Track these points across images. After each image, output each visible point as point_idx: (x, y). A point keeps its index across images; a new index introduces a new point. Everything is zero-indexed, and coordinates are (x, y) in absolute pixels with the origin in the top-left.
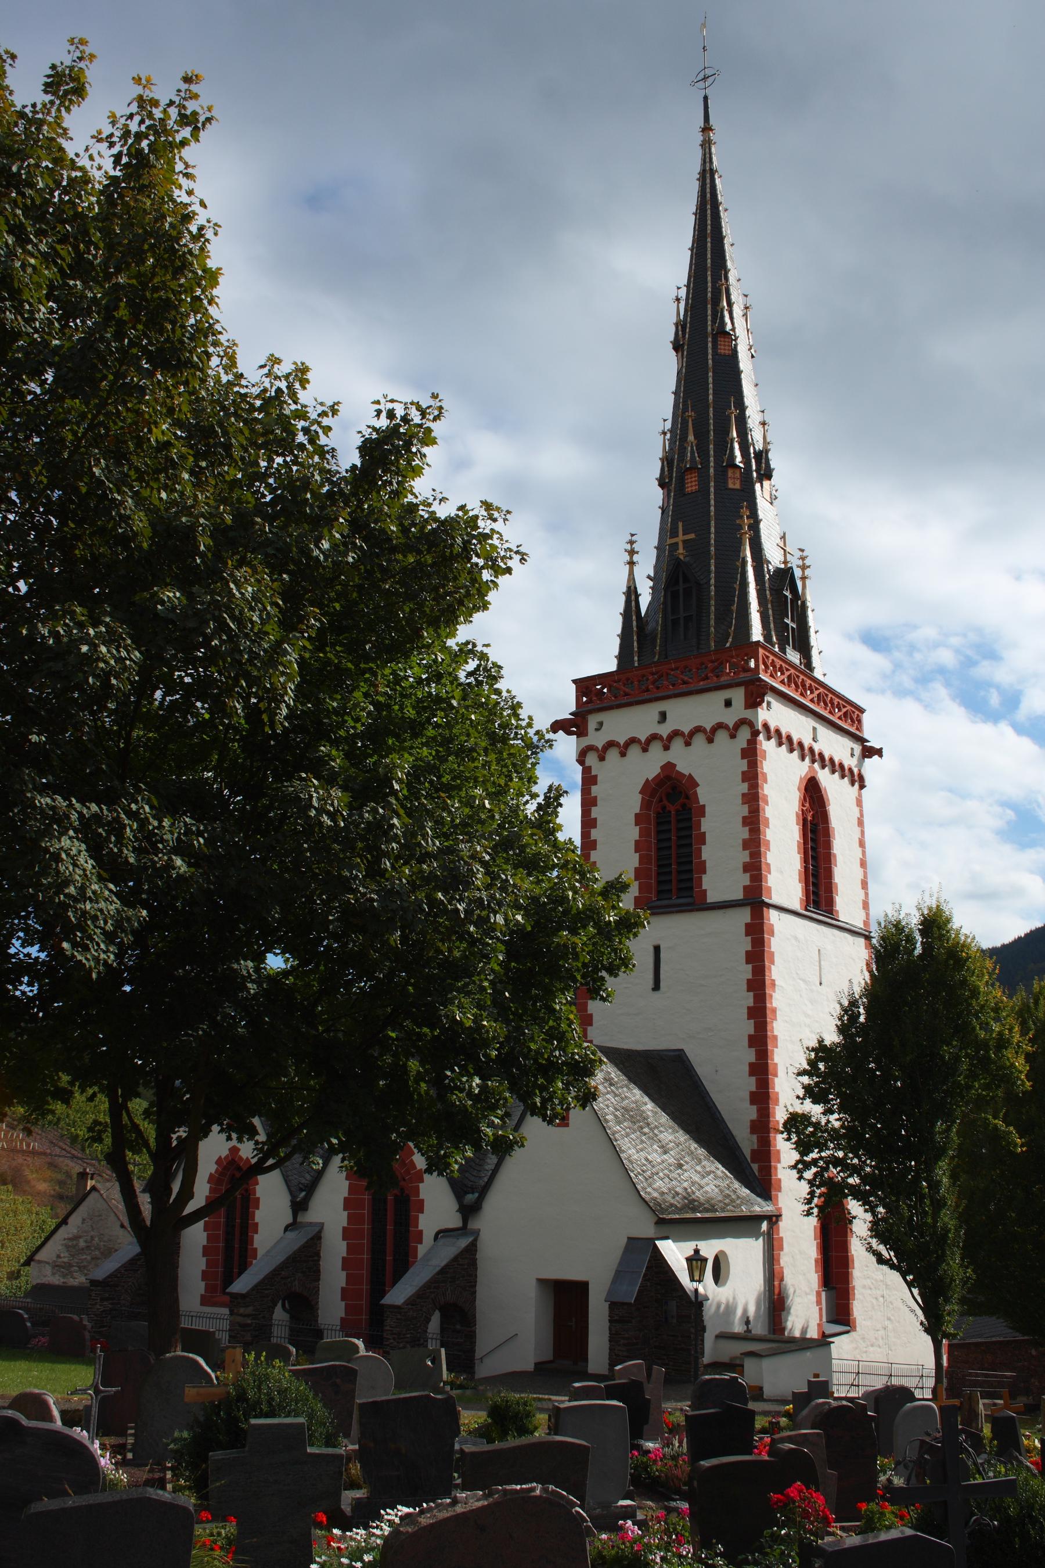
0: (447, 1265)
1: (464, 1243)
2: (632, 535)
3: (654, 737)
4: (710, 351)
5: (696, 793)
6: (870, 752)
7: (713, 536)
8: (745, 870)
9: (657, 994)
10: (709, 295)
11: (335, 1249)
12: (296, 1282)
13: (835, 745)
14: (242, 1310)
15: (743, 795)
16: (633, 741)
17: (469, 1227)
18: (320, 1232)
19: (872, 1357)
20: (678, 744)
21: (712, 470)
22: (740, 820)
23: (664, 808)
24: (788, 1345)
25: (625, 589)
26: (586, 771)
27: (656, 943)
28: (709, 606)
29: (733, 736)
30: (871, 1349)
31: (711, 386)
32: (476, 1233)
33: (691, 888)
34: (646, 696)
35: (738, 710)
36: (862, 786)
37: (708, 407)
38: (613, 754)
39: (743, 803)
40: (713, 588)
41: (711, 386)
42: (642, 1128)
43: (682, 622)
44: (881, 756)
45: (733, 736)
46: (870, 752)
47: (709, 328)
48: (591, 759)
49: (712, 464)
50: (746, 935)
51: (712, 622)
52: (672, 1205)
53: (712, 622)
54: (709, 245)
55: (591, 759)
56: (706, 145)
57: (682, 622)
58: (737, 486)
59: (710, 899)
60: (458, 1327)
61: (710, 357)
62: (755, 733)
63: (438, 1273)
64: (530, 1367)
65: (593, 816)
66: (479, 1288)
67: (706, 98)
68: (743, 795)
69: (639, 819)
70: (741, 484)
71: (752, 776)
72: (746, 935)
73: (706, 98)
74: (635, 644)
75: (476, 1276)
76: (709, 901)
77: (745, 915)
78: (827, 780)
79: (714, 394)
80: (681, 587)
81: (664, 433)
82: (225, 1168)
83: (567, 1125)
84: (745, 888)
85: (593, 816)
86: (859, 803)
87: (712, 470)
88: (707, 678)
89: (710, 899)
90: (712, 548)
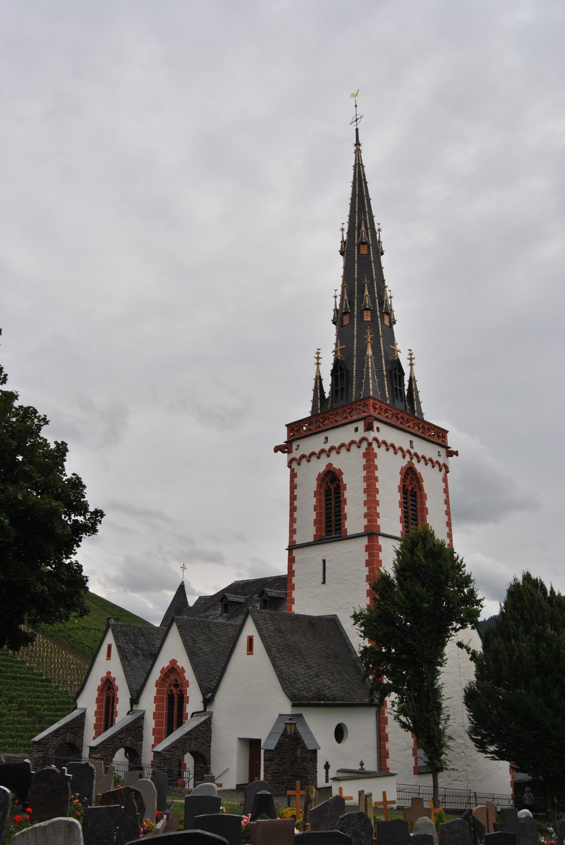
0: (191, 731)
1: (203, 719)
2: (318, 349)
3: (323, 451)
4: (356, 253)
5: (342, 478)
6: (451, 454)
7: (355, 346)
8: (365, 516)
9: (324, 586)
10: (357, 225)
11: (150, 724)
12: (128, 741)
13: (423, 448)
14: (94, 756)
15: (364, 477)
16: (313, 454)
17: (207, 710)
18: (143, 714)
19: (456, 787)
20: (333, 453)
21: (356, 312)
22: (363, 490)
23: (328, 487)
24: (363, 775)
25: (314, 377)
26: (292, 471)
27: (324, 558)
28: (353, 381)
29: (359, 447)
30: (455, 782)
31: (356, 270)
32: (211, 714)
33: (341, 529)
34: (319, 430)
35: (361, 433)
36: (447, 472)
37: (354, 281)
38: (304, 461)
39: (364, 482)
40: (355, 372)
41: (356, 270)
42: (295, 655)
43: (340, 391)
44: (457, 455)
45: (359, 447)
46: (451, 454)
47: (356, 241)
48: (294, 465)
49: (356, 309)
50: (366, 551)
51: (354, 390)
52: (304, 696)
53: (354, 390)
54: (357, 200)
55: (294, 465)
56: (358, 152)
57: (340, 391)
58: (369, 319)
59: (349, 533)
60: (202, 765)
61: (356, 256)
62: (370, 444)
63: (185, 735)
64: (234, 787)
65: (295, 494)
66: (212, 744)
67: (357, 130)
68: (364, 477)
69: (316, 494)
70: (371, 318)
71: (370, 467)
72: (366, 551)
73: (357, 130)
74: (319, 404)
75: (211, 737)
76: (348, 534)
77: (364, 541)
78: (420, 467)
79: (358, 274)
80: (339, 373)
81: (336, 297)
82: (105, 683)
83: (252, 654)
84: (365, 526)
85: (295, 494)
86: (445, 480)
87: (356, 312)
88: (346, 418)
89: (349, 533)
90: (355, 352)
